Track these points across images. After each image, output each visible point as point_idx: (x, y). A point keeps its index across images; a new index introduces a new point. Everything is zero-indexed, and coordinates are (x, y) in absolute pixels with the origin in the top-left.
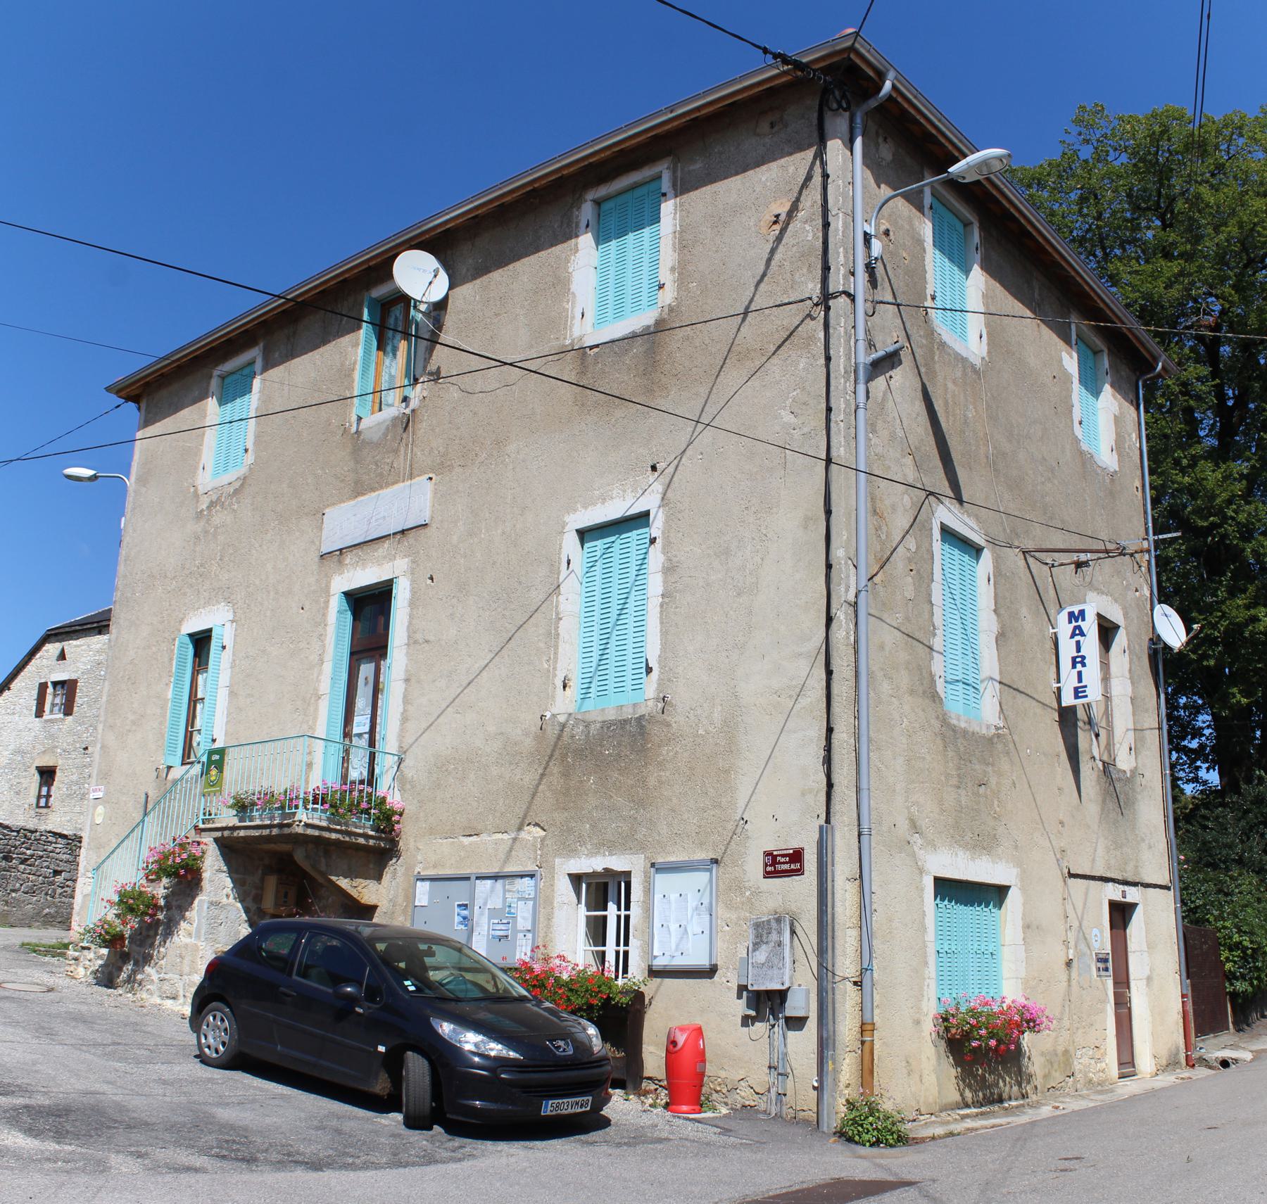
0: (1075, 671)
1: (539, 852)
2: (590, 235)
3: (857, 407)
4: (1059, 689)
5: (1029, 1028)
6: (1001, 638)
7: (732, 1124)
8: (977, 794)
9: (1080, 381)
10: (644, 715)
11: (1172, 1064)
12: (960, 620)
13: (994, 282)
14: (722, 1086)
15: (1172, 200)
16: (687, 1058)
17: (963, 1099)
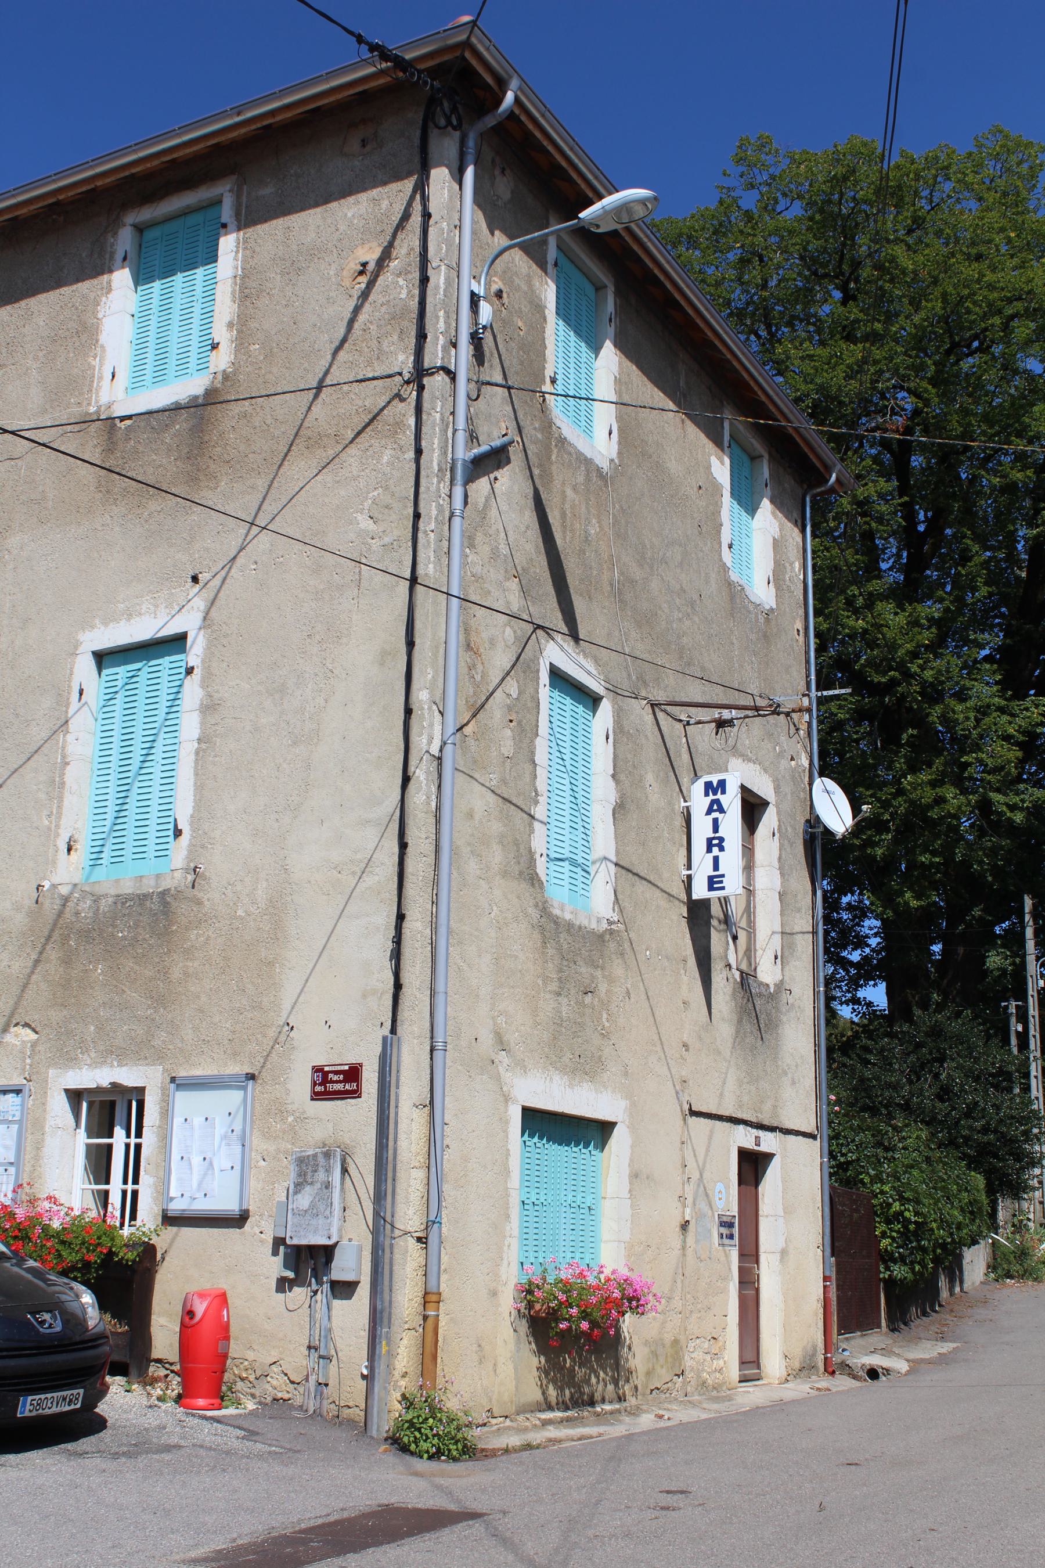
0: (710, 856)
1: (28, 1061)
2: (127, 271)
3: (452, 515)
4: (689, 877)
5: (631, 1308)
6: (619, 810)
7: (258, 1425)
8: (581, 1004)
9: (733, 495)
10: (169, 890)
11: (805, 1369)
12: (569, 786)
13: (629, 364)
14: (250, 1371)
15: (856, 265)
16: (206, 1332)
17: (546, 1399)
